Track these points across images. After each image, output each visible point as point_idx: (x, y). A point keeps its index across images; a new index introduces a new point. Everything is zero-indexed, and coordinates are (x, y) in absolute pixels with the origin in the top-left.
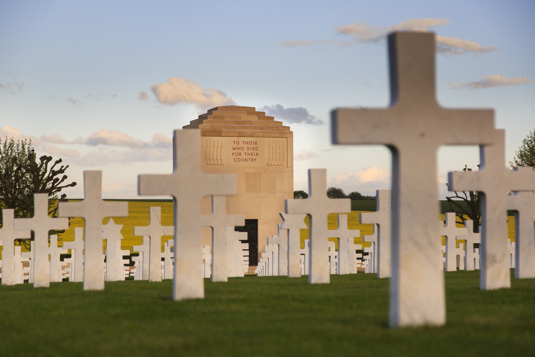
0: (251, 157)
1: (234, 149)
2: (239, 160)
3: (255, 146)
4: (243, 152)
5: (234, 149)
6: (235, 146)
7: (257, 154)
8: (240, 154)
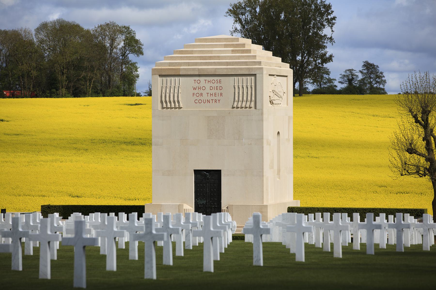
0: (214, 98)
1: (195, 89)
2: (200, 101)
3: (219, 85)
4: (204, 93)
5: (195, 89)
6: (196, 85)
7: (221, 94)
8: (202, 94)
